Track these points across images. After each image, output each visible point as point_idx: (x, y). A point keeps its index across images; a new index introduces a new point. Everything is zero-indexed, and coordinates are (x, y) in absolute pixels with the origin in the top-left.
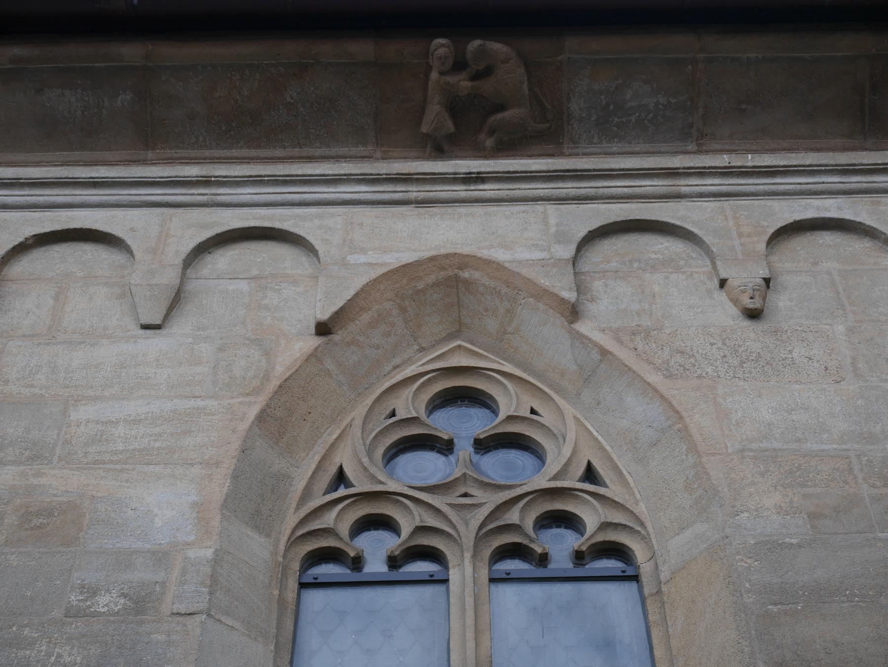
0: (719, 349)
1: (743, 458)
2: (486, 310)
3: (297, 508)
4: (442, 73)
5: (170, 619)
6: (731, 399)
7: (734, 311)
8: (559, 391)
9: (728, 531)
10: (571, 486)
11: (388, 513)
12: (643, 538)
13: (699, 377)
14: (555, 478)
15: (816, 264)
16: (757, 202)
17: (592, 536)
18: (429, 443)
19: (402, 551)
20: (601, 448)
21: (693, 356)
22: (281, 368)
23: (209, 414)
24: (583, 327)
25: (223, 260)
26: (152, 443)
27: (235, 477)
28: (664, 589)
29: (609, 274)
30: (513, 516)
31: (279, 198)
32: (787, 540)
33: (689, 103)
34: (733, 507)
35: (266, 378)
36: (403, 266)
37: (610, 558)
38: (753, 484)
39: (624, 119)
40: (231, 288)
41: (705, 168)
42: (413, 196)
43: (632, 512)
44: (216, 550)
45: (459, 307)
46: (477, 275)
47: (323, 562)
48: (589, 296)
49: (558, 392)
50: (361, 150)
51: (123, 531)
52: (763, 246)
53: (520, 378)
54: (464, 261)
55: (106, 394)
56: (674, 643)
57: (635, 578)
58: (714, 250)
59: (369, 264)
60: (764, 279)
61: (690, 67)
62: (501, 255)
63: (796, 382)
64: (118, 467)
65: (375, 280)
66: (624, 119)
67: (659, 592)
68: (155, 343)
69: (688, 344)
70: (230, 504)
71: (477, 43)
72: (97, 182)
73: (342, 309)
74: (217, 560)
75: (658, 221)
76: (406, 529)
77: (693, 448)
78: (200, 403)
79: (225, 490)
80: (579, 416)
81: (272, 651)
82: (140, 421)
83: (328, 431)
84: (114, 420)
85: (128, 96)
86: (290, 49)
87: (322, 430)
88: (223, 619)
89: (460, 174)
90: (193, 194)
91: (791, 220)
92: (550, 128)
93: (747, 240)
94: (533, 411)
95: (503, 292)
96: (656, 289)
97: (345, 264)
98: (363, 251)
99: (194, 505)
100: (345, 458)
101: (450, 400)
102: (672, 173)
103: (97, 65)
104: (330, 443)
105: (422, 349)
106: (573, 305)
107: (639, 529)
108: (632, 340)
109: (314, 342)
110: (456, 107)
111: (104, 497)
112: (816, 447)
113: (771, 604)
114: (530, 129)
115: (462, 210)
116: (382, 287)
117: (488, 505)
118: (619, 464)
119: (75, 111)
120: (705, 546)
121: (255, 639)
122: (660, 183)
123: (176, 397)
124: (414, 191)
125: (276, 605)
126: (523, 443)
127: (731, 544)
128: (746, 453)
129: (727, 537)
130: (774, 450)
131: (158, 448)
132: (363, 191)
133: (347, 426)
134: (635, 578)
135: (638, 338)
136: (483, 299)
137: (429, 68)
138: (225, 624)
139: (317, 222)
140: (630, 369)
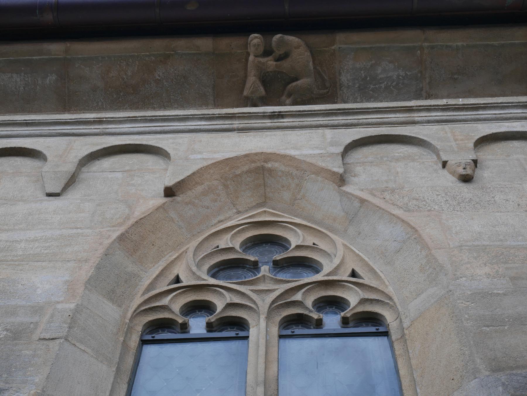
0: (442, 197)
1: (461, 250)
2: (283, 187)
3: (143, 294)
4: (256, 56)
5: (38, 342)
6: (452, 221)
7: (454, 179)
9: (451, 287)
10: (339, 279)
11: (208, 299)
12: (391, 307)
13: (429, 211)
14: (328, 275)
15: (509, 156)
16: (466, 125)
17: (354, 308)
18: (241, 265)
19: (217, 320)
20: (362, 260)
21: (425, 201)
22: (139, 212)
23: (85, 236)
25: (107, 163)
26: (43, 251)
27: (98, 268)
28: (406, 332)
29: (366, 164)
31: (147, 129)
32: (495, 291)
33: (419, 75)
34: (455, 275)
36: (227, 159)
37: (369, 323)
38: (469, 263)
39: (377, 86)
40: (110, 176)
41: (430, 106)
42: (235, 126)
43: (383, 292)
44: (78, 305)
45: (265, 187)
46: (276, 165)
47: (161, 330)
48: (353, 174)
49: (331, 231)
51: (13, 296)
52: (471, 145)
53: (306, 226)
55: (16, 227)
56: (414, 362)
57: (386, 334)
58: (438, 147)
59: (204, 159)
60: (473, 160)
61: (419, 51)
62: (292, 153)
63: (498, 212)
64: (16, 263)
65: (207, 167)
66: (377, 86)
67: (403, 335)
69: (421, 195)
70: (92, 283)
71: (278, 36)
72: (29, 123)
73: (183, 181)
74: (78, 310)
75: (400, 135)
77: (425, 246)
78: (79, 231)
79: (90, 274)
80: (346, 243)
81: (113, 371)
82: (36, 240)
83: (170, 254)
84: (19, 240)
85: (54, 77)
86: (158, 45)
87: (166, 253)
88: (77, 344)
89: (267, 113)
90: (91, 129)
91: (491, 133)
92: (328, 92)
93: (461, 142)
94: (314, 244)
95: (294, 174)
96: (399, 170)
97: (187, 159)
98: (200, 153)
99: (67, 281)
100: (180, 270)
101: (258, 244)
102: (410, 110)
103: (34, 58)
104: (170, 260)
105: (239, 212)
106: (341, 175)
107: (388, 301)
108: (381, 194)
110: (266, 80)
111: (3, 279)
112: (513, 243)
113: (484, 326)
114: (315, 92)
115: (268, 133)
116: (212, 171)
117: (279, 290)
118: (374, 267)
119: (20, 87)
120: (435, 300)
121: (101, 362)
122: (401, 116)
123: (64, 228)
124: (236, 124)
125: (120, 346)
126: (307, 264)
127: (453, 294)
128: (463, 248)
129: (451, 291)
130: (484, 245)
131: (46, 254)
133: (183, 252)
134: (386, 334)
135: (386, 193)
136: (281, 180)
137: (248, 54)
138: (78, 347)
139: (171, 141)
140: (380, 208)
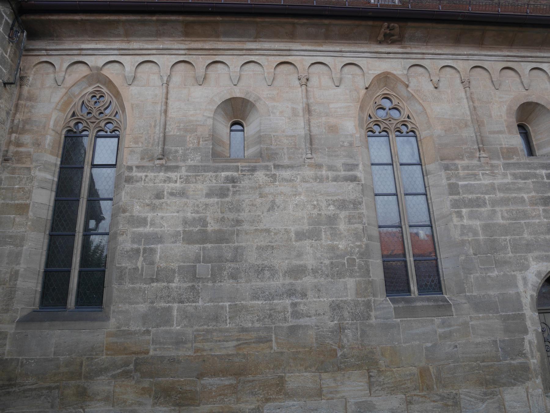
7: (433, 86)
8: (403, 100)
24: (409, 89)
35: (359, 99)
54: (388, 73)
62: (395, 72)
68: (338, 90)
76: (382, 128)
77: (427, 116)
86: (357, 22)
97: (368, 73)
102: (423, 54)
109: (365, 91)
110: (385, 35)
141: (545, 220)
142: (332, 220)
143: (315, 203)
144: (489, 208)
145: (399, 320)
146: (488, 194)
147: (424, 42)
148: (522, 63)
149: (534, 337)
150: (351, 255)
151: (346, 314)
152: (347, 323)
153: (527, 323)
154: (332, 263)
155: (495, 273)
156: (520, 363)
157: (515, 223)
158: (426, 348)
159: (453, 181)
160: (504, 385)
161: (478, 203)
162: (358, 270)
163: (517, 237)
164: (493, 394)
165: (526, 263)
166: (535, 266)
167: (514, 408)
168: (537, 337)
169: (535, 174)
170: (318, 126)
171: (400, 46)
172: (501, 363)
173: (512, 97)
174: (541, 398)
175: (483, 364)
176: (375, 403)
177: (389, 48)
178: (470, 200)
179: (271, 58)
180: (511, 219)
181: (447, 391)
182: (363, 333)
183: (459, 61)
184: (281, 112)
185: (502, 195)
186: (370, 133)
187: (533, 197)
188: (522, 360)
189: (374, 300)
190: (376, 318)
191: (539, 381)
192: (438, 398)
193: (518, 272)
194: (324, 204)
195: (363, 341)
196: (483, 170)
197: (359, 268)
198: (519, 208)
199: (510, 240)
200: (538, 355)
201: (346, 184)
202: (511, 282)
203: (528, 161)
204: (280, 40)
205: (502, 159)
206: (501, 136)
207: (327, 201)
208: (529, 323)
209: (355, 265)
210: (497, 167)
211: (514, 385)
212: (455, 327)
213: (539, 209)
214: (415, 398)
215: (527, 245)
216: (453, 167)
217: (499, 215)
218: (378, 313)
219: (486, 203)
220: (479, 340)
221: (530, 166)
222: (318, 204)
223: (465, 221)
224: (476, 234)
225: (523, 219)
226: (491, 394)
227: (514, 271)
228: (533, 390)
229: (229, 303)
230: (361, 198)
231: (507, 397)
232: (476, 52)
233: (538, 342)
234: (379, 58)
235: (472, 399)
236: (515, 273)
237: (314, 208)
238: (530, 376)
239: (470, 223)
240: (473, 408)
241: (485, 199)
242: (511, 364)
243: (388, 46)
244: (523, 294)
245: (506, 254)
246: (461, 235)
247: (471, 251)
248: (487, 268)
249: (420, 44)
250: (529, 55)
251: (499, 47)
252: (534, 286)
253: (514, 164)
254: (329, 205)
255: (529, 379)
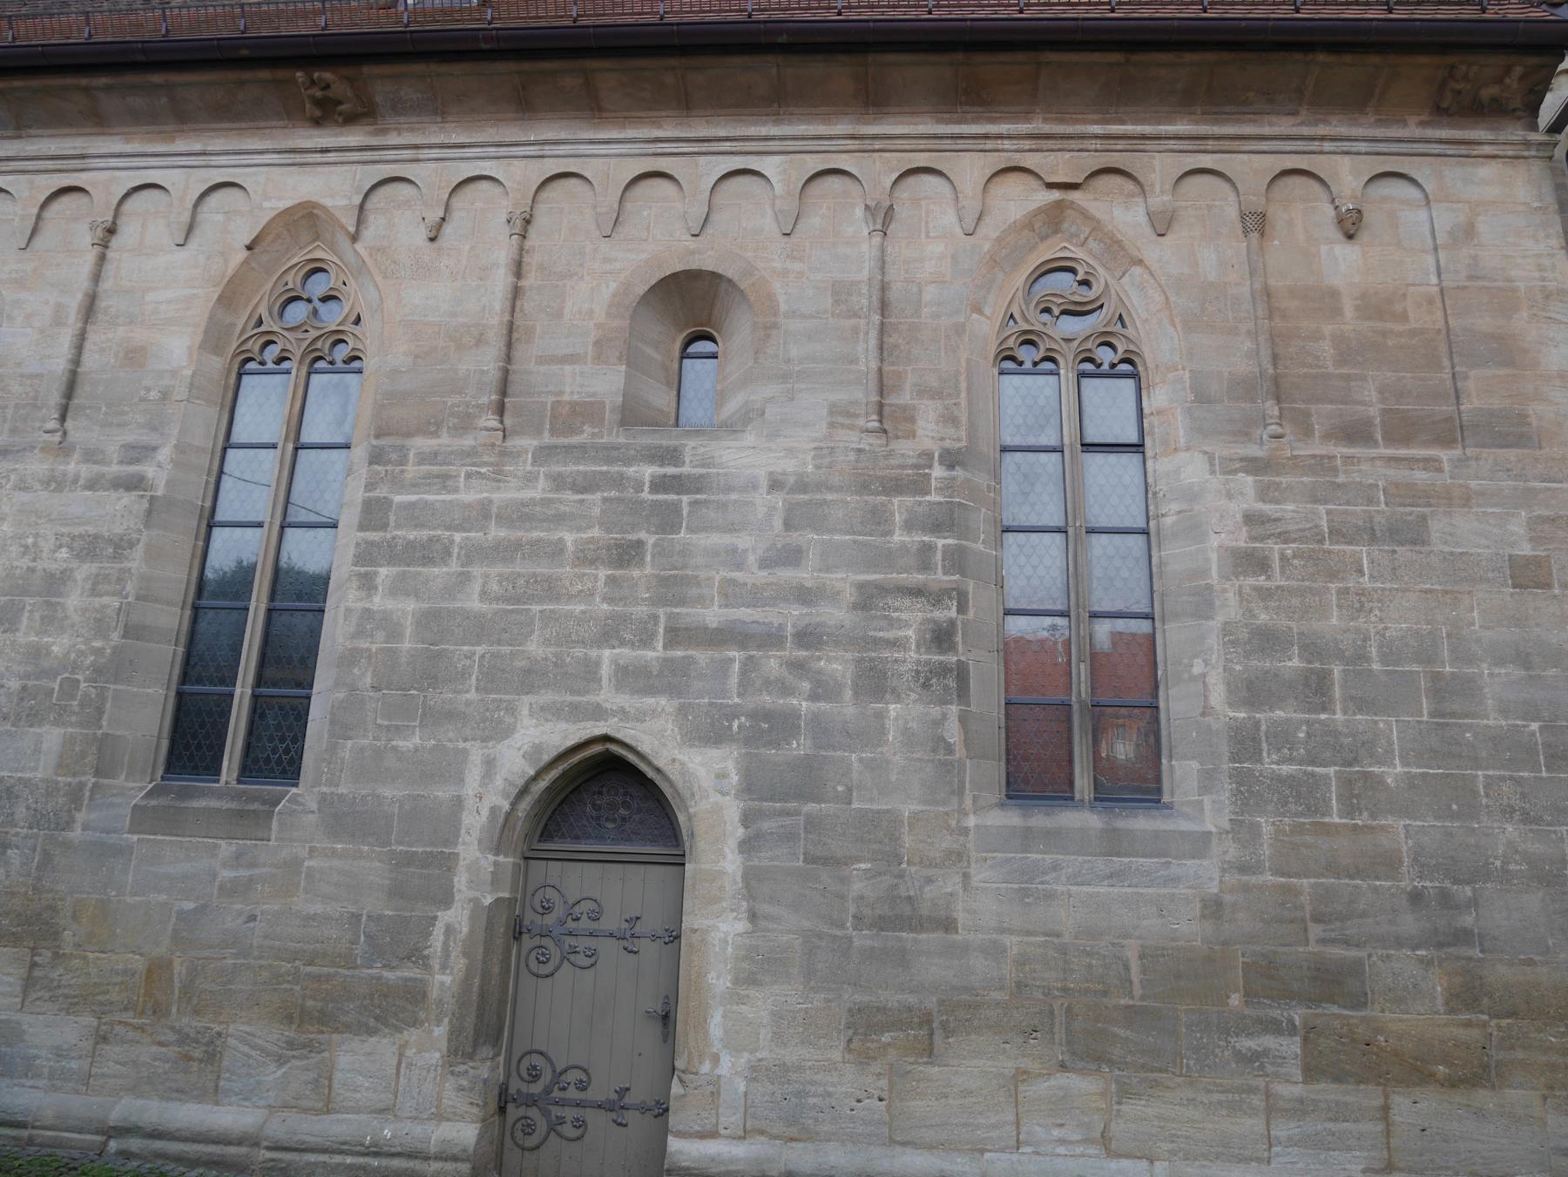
24: (358, 246)
30: (319, 345)
50: (281, 123)
54: (315, 205)
62: (328, 202)
68: (182, 254)
70: (203, 346)
74: (193, 376)
100: (263, 310)
102: (416, 147)
110: (318, 103)
115: (319, 169)
132: (274, 158)
141: (605, 606)
142: (55, 583)
143: (30, 541)
144: (454, 566)
145: (135, 837)
146: (465, 530)
147: (436, 113)
148: (702, 159)
149: (465, 918)
150: (73, 672)
151: (21, 812)
152: (17, 834)
153: (456, 880)
154: (24, 688)
155: (411, 742)
156: (406, 979)
157: (512, 611)
158: (180, 913)
159: (381, 492)
160: (347, 1028)
161: (428, 553)
162: (77, 709)
163: (506, 649)
164: (309, 1046)
165: (508, 719)
166: (532, 731)
167: (355, 1091)
168: (472, 918)
169: (622, 475)
170: (102, 350)
171: (367, 128)
172: (356, 972)
173: (644, 256)
174: (432, 1075)
175: (309, 969)
176: (25, 1027)
177: (341, 134)
178: (411, 545)
179: (41, 179)
180: (507, 600)
181: (198, 1024)
182: (47, 857)
183: (516, 162)
184: (28, 317)
185: (503, 533)
186: (1089, 367)
187: (591, 541)
188: (410, 972)
189: (95, 785)
190: (85, 827)
191: (440, 1031)
192: (171, 1037)
193: (478, 744)
194: (46, 546)
195: (39, 879)
196: (474, 464)
197: (81, 705)
198: (539, 570)
199: (483, 656)
200: (459, 963)
201: (114, 495)
202: (452, 768)
203: (622, 440)
204: (74, 131)
205: (546, 434)
206: (568, 368)
207: (58, 536)
208: (461, 881)
209: (73, 697)
210: (516, 455)
211: (372, 1032)
212: (265, 870)
213: (596, 576)
214: (118, 1028)
215: (529, 671)
216: (394, 456)
217: (477, 587)
218: (93, 816)
219: (450, 554)
220: (317, 908)
221: (615, 453)
222: (35, 544)
223: (377, 599)
224: (394, 634)
225: (541, 600)
226: (304, 1047)
227: (466, 740)
228: (419, 1052)
229: (1327, 820)
230: (139, 531)
231: (344, 1060)
232: (563, 135)
233: (471, 932)
234: (301, 165)
235: (253, 1053)
236: (468, 745)
237: (24, 554)
238: (422, 1015)
239: (390, 604)
240: (249, 1075)
241: (452, 542)
242: (379, 978)
243: (339, 130)
244: (470, 803)
245: (459, 692)
246: (353, 637)
247: (368, 680)
248: (397, 727)
249: (425, 119)
250: (722, 133)
251: (650, 114)
252: (511, 784)
253: (582, 448)
254: (61, 546)
255: (415, 1023)
